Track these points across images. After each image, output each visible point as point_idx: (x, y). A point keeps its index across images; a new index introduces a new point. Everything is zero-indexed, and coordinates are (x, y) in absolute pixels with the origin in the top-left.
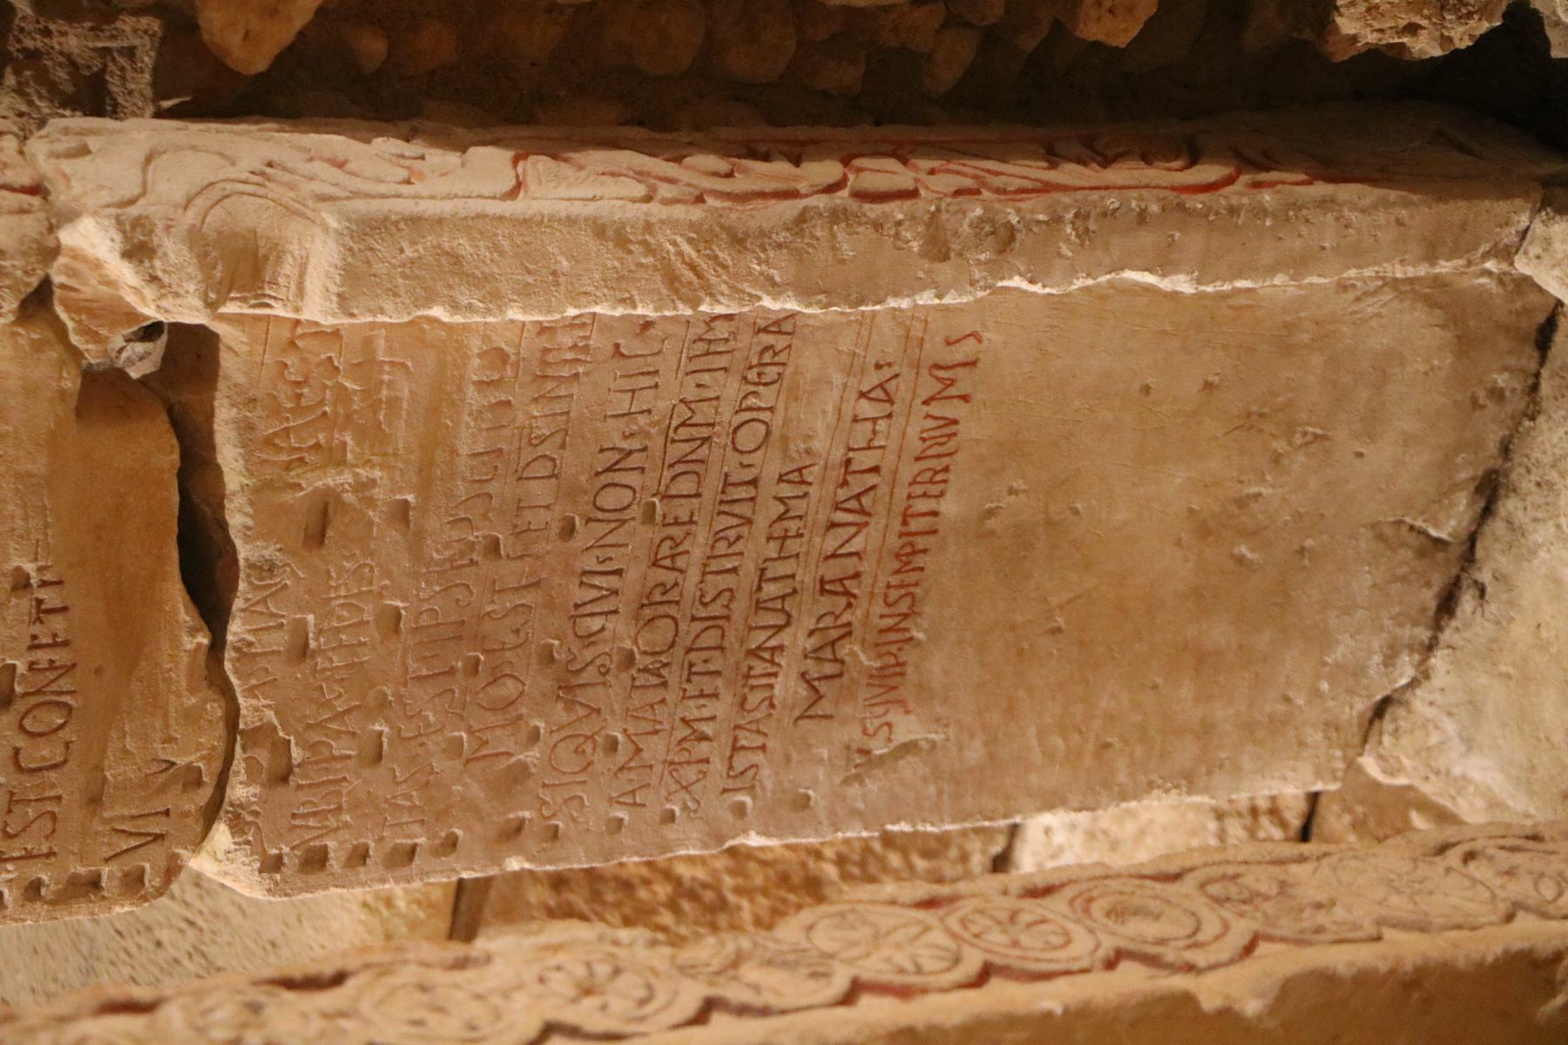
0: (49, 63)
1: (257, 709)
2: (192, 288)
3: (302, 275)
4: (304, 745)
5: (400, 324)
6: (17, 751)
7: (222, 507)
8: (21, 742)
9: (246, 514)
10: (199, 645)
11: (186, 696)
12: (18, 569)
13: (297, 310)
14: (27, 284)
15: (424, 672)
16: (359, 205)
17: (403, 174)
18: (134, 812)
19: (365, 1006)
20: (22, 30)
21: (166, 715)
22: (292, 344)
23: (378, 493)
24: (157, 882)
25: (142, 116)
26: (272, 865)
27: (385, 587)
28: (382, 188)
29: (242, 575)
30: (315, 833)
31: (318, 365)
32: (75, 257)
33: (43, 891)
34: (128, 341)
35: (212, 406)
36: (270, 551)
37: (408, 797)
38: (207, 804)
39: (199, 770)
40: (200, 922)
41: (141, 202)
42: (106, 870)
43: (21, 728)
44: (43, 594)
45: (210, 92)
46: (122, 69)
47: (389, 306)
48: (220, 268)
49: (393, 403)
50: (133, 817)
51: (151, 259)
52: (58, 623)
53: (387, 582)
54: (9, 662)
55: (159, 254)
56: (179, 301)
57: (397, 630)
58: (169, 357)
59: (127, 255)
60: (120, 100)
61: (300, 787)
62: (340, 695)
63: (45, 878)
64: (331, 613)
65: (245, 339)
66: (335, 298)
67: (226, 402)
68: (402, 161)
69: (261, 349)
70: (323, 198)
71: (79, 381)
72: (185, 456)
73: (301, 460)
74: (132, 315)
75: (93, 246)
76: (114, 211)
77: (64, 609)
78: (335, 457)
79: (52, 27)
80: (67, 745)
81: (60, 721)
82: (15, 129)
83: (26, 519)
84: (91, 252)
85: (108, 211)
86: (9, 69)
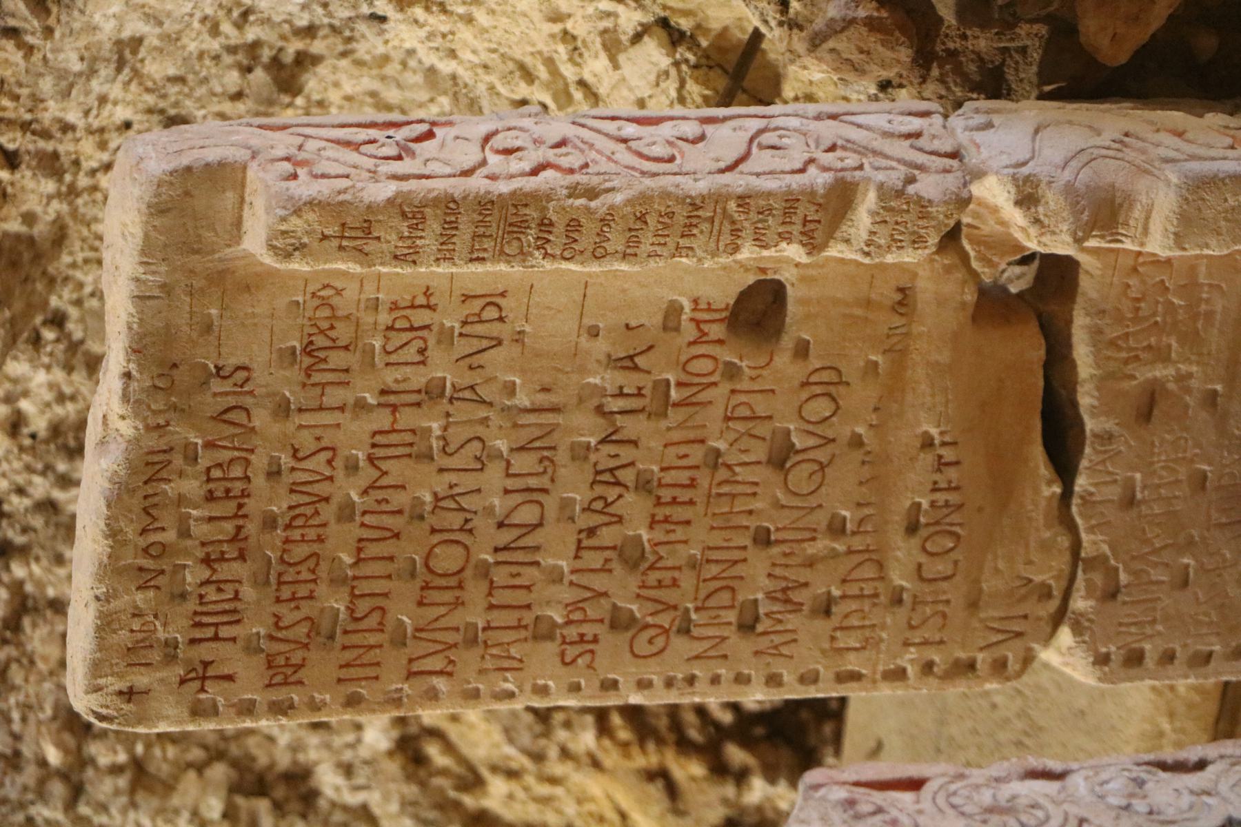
0: (963, 59)
1: (1095, 543)
2: (1065, 228)
3: (1148, 218)
4: (1128, 570)
5: (1220, 257)
6: (920, 566)
7: (1074, 391)
8: (923, 559)
9: (1093, 397)
10: (1054, 493)
11: (1043, 530)
12: (926, 433)
13: (1142, 244)
14: (946, 225)
15: (1224, 520)
16: (1195, 166)
17: (1229, 141)
18: (1003, 615)
19: (1223, 787)
20: (947, 36)
21: (1027, 546)
22: (1135, 270)
23: (1194, 383)
24: (1017, 667)
25: (1028, 98)
26: (1102, 660)
27: (1196, 455)
28: (1212, 153)
29: (1088, 442)
30: (1135, 638)
31: (1153, 285)
32: (979, 204)
33: (935, 669)
34: (1009, 264)
35: (1071, 316)
36: (1109, 425)
37: (1207, 614)
38: (1056, 613)
39: (1050, 587)
40: (1027, 692)
41: (1030, 164)
42: (980, 656)
43: (924, 549)
44: (943, 451)
45: (1079, 78)
46: (1017, 63)
47: (1213, 243)
48: (1086, 213)
49: (1209, 315)
50: (1002, 619)
51: (1036, 206)
52: (952, 473)
53: (1197, 451)
54: (917, 500)
55: (1043, 201)
56: (1054, 238)
57: (1203, 488)
58: (1039, 278)
59: (1018, 203)
60: (1013, 86)
61: (1125, 603)
62: (1158, 536)
63: (937, 659)
64: (1155, 472)
65: (1099, 266)
66: (1172, 236)
67: (1082, 312)
68: (1228, 131)
69: (1110, 272)
70: (1167, 161)
71: (976, 296)
72: (1050, 351)
73: (1137, 358)
74: (1018, 247)
75: (994, 196)
76: (1011, 171)
77: (957, 463)
78: (1162, 356)
79: (969, 33)
80: (956, 563)
81: (951, 545)
82: (941, 110)
83: (933, 396)
84: (991, 200)
85: (1006, 171)
86: (935, 64)
